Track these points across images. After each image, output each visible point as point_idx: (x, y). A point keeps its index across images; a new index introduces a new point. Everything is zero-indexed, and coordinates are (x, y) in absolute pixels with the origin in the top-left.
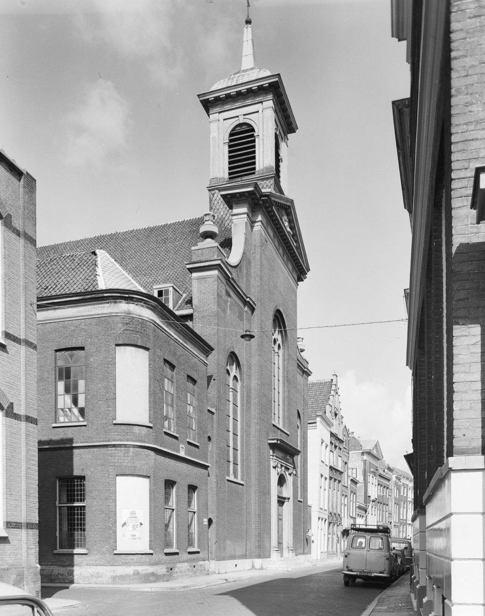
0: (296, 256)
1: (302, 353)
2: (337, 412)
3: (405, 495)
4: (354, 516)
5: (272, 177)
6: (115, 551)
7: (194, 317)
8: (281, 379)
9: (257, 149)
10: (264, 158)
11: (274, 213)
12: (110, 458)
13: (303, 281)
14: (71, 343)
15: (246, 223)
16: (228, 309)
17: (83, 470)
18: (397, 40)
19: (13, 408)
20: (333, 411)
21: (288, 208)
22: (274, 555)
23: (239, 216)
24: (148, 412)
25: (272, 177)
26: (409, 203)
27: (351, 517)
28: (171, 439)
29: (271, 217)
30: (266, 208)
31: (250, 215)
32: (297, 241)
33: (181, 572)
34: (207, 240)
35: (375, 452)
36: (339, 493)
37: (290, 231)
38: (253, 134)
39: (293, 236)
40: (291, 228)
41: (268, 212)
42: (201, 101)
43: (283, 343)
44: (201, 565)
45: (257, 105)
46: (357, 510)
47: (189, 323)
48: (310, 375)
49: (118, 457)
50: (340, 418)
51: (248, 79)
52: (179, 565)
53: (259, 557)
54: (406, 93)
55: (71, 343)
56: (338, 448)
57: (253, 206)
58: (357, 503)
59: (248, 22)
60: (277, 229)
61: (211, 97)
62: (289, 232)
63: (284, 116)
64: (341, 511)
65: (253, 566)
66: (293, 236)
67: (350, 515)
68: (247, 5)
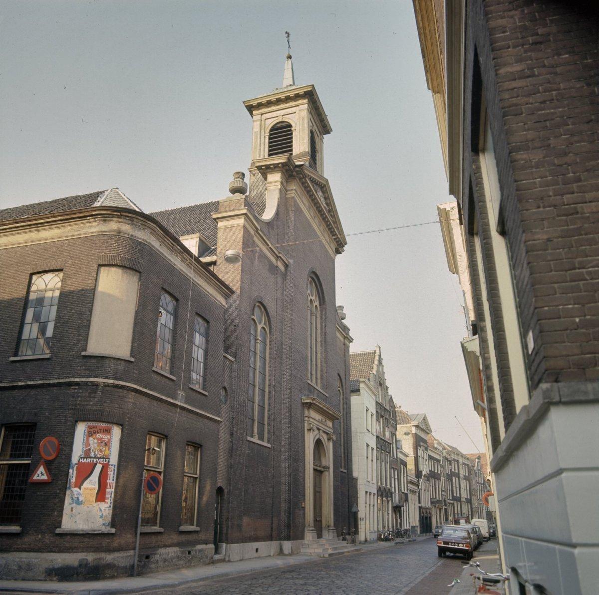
1: (343, 321)
3: (457, 471)
4: (406, 492)
6: (58, 529)
7: (218, 263)
8: (319, 340)
9: (294, 140)
10: (300, 145)
12: (71, 399)
13: (341, 253)
14: (49, 265)
15: (462, 562)
16: (257, 259)
17: (36, 414)
20: (377, 381)
21: (324, 187)
22: (309, 536)
23: (273, 184)
24: (130, 344)
27: (402, 493)
28: (199, 396)
29: (306, 188)
30: (300, 179)
31: (285, 184)
32: (333, 216)
33: (165, 560)
34: (236, 194)
35: (424, 427)
36: (388, 465)
39: (329, 211)
40: (326, 204)
41: (303, 183)
42: (246, 106)
43: (320, 305)
44: (200, 551)
45: (295, 108)
46: (409, 485)
47: (211, 268)
48: (351, 342)
49: (81, 397)
50: (385, 388)
52: (162, 551)
53: (288, 538)
55: (49, 265)
57: (287, 176)
58: (409, 478)
59: (290, 57)
60: (313, 200)
61: (255, 103)
62: (324, 207)
63: (320, 120)
64: (391, 486)
65: (281, 549)
67: (401, 490)
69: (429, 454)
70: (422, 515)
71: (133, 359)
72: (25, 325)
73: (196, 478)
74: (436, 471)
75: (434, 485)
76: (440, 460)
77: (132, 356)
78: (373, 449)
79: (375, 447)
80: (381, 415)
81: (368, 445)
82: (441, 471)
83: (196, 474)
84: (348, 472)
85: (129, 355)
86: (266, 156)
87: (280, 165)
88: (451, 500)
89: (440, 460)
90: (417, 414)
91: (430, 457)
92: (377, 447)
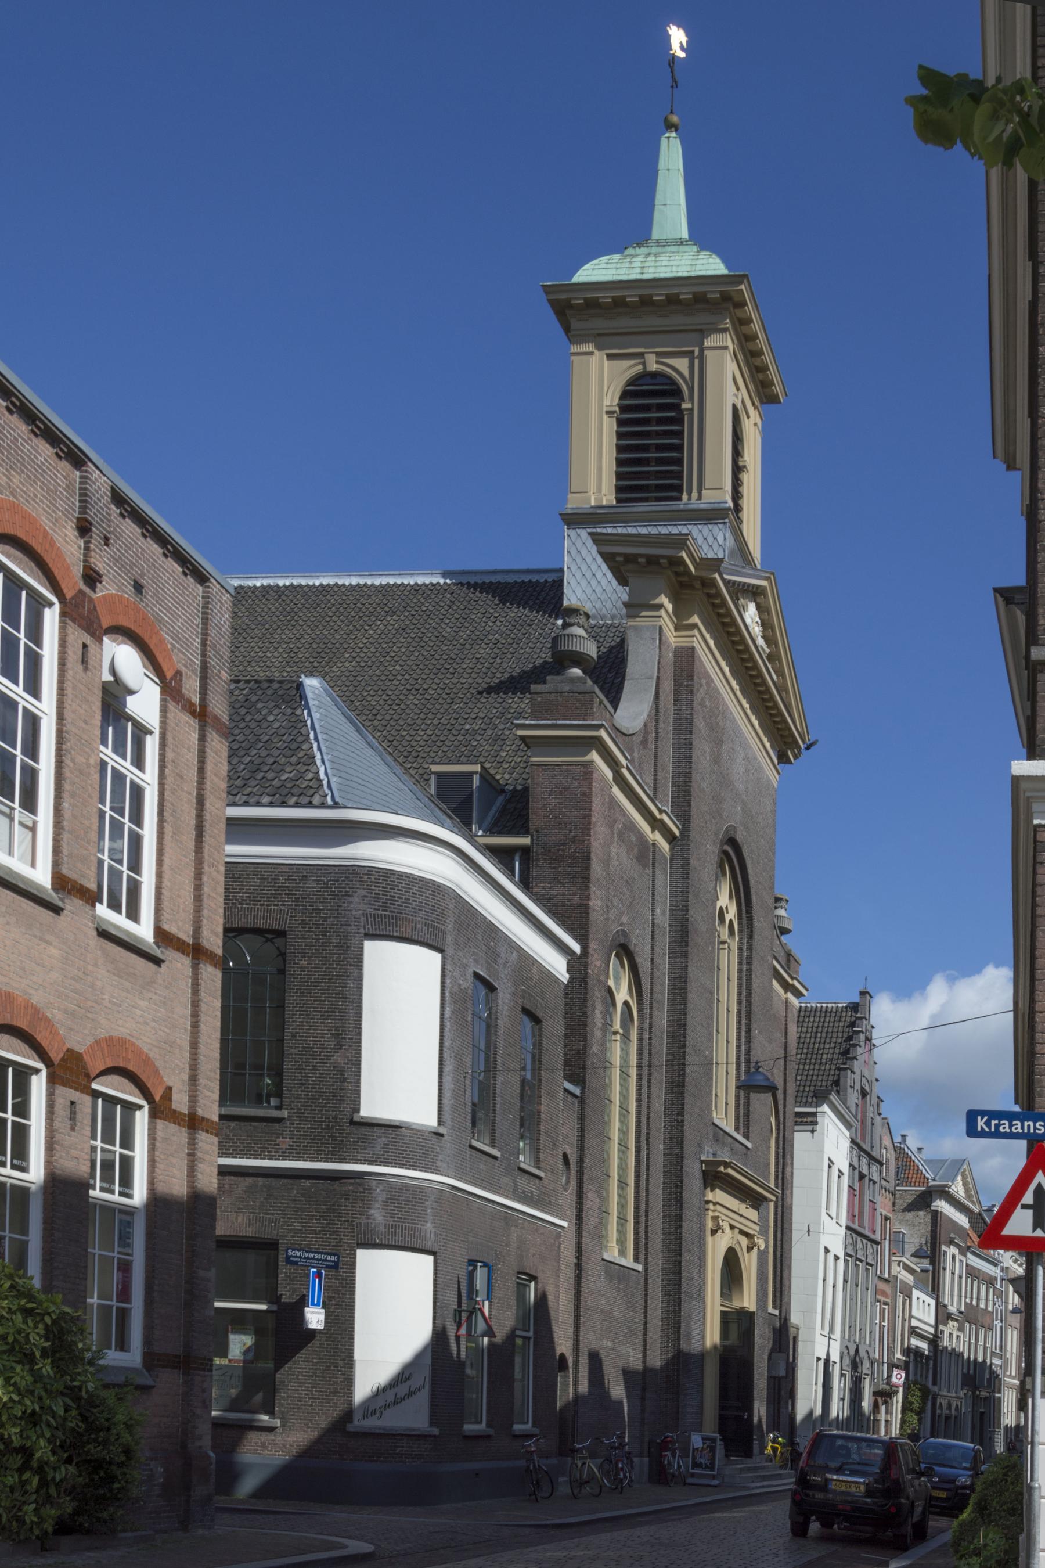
0: (776, 706)
2: (867, 1088)
5: (748, 1098)
11: (724, 600)
18: (1005, 466)
19: (170, 1100)
25: (748, 1098)
26: (1024, 747)
37: (765, 646)
38: (680, 405)
42: (549, 300)
50: (875, 1101)
51: (669, 269)
54: (1018, 578)
56: (866, 1179)
66: (770, 657)
68: (670, 82)
69: (969, 1262)
70: (938, 1411)
71: (436, 1431)
72: (1012, 1009)
73: (529, 1338)
74: (982, 1306)
75: (973, 1341)
76: (996, 1279)
77: (432, 1423)
78: (837, 1258)
79: (841, 1255)
80: (860, 1173)
81: (827, 1250)
82: (994, 1304)
83: (528, 1331)
84: (780, 1312)
85: (427, 1425)
86: (608, 497)
87: (618, 559)
88: (1014, 1378)
89: (996, 1279)
90: (848, 1142)
91: (973, 1273)
92: (847, 1254)
